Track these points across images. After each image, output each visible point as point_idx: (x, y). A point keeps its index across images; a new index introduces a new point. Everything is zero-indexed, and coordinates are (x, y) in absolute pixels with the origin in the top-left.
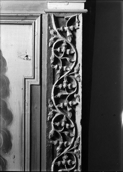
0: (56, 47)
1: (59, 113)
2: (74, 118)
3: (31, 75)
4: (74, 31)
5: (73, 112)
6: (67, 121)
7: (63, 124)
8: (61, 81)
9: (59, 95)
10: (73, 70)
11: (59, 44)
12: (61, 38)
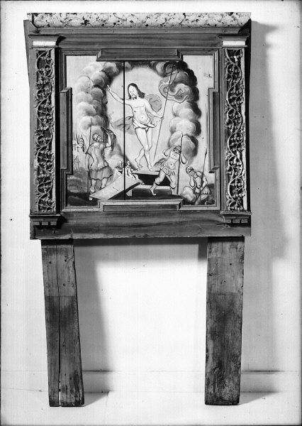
0: (229, 68)
1: (232, 108)
2: (240, 111)
3: (212, 86)
4: (239, 59)
5: (240, 107)
6: (237, 114)
7: (235, 162)
8: (234, 182)
9: (231, 98)
10: (239, 82)
11: (232, 111)
12: (232, 63)
